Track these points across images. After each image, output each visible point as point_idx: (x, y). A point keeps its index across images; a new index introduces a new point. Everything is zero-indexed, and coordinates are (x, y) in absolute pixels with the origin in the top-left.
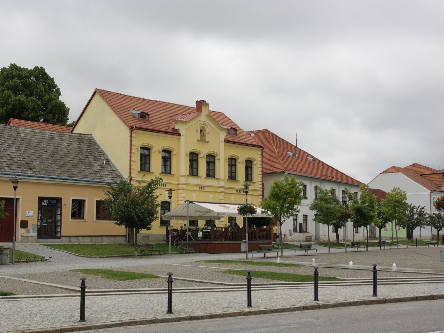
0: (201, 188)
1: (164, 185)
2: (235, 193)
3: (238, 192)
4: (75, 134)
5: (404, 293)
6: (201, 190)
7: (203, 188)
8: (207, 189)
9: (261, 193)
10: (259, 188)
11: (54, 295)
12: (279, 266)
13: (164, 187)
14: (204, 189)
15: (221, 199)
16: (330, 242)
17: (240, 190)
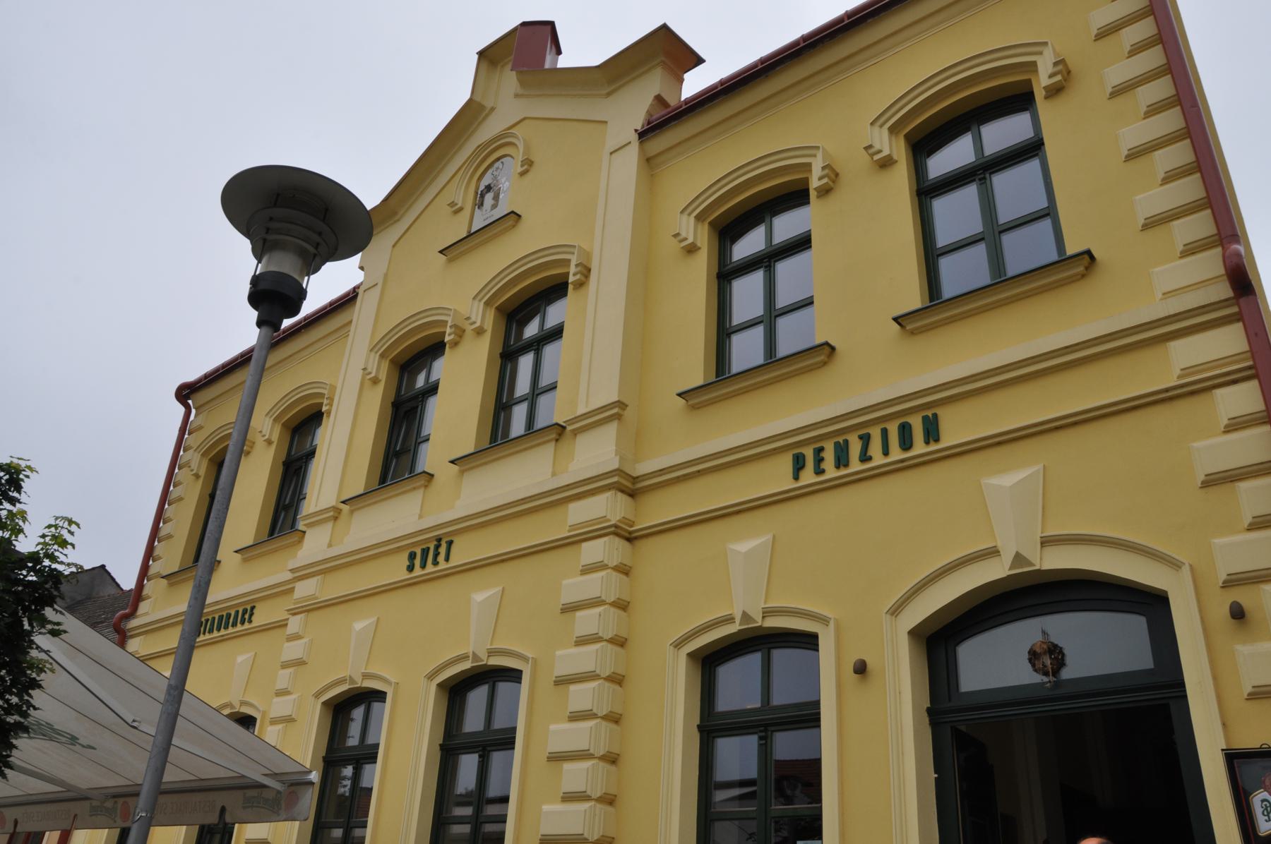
0: (417, 562)
7: (437, 554)
14: (441, 558)
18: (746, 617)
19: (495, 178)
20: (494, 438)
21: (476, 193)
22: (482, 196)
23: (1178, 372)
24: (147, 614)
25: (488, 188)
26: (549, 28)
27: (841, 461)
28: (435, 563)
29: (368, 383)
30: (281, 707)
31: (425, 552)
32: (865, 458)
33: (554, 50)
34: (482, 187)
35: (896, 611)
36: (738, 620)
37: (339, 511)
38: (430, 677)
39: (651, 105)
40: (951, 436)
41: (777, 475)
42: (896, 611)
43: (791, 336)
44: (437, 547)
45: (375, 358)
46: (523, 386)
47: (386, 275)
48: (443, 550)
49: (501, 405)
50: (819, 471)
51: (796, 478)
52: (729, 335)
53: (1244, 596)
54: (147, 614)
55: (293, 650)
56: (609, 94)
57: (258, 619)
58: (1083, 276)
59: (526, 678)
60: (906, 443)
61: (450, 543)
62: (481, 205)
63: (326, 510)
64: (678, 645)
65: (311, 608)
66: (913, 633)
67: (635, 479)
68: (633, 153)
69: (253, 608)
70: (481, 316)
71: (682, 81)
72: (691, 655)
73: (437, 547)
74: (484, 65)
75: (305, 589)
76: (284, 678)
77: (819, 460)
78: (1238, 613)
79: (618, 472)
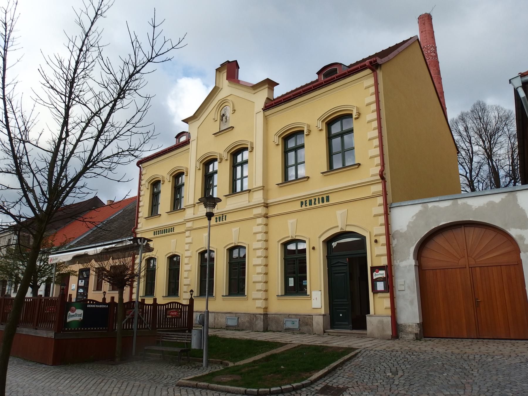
0: (218, 220)
1: (172, 230)
2: (300, 208)
3: (308, 204)
4: (224, 73)
5: (80, 100)
6: (156, 236)
7: (223, 219)
8: (229, 218)
9: (379, 188)
10: (372, 176)
11: (97, 245)
12: (61, 293)
13: (173, 232)
14: (224, 219)
15: (378, 253)
16: (211, 332)
17: (313, 199)
18: (292, 237)
19: (225, 112)
20: (233, 192)
21: (220, 116)
22: (222, 117)
23: (372, 193)
24: (141, 228)
25: (224, 115)
26: (235, 62)
27: (311, 204)
28: (223, 220)
29: (197, 170)
30: (188, 254)
31: (220, 218)
32: (315, 204)
33: (237, 68)
34: (222, 114)
35: (320, 237)
36: (290, 237)
37: (195, 205)
38: (225, 247)
39: (266, 100)
40: (331, 201)
41: (297, 206)
42: (320, 237)
43: (302, 172)
44: (223, 217)
45: (198, 163)
46: (239, 175)
47: (197, 137)
48: (224, 217)
49: (234, 180)
50: (306, 206)
51: (302, 207)
52: (288, 168)
53: (377, 238)
54: (141, 228)
55: (189, 240)
56: (254, 94)
57: (176, 231)
58: (358, 168)
59: (215, 252)
60: (323, 202)
61: (226, 216)
62: (222, 120)
63: (191, 205)
64: (279, 242)
65: (191, 230)
66: (323, 242)
67: (267, 204)
68: (261, 115)
69: (174, 228)
70: (226, 156)
71: (273, 90)
72: (281, 244)
73: (223, 217)
74: (218, 72)
75: (189, 225)
76: (187, 246)
77: (306, 203)
78: (376, 241)
79: (264, 203)
